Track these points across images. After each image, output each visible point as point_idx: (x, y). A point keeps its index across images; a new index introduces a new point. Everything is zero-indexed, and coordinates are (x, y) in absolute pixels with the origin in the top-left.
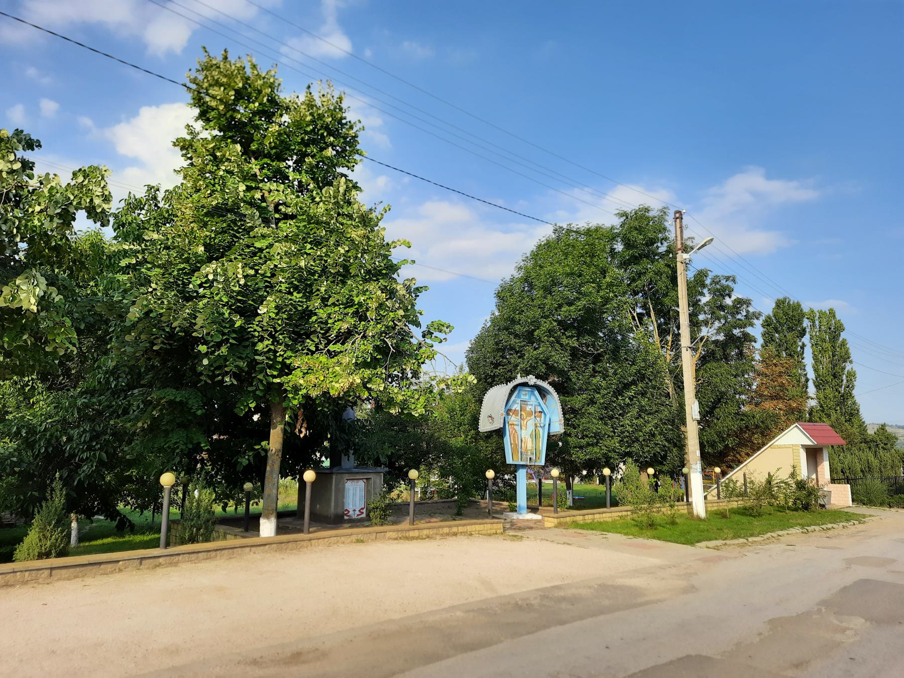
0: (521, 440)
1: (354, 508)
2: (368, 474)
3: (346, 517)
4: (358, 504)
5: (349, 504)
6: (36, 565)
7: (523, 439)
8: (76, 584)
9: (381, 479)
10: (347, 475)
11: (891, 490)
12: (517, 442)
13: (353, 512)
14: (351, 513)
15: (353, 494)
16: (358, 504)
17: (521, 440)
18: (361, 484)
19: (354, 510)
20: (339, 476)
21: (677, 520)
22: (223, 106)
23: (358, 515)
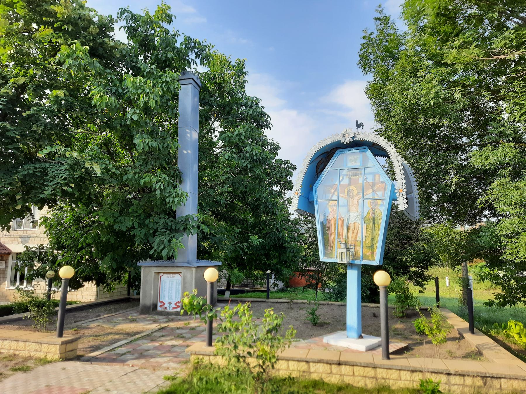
0: (348, 227)
1: (170, 301)
2: (178, 269)
3: (159, 309)
4: (174, 297)
5: (164, 296)
6: (139, 326)
7: (352, 226)
8: (349, 360)
9: (192, 274)
10: (155, 268)
11: (251, 315)
12: (340, 231)
13: (168, 305)
14: (167, 305)
15: (169, 288)
16: (174, 297)
17: (348, 227)
18: (178, 278)
19: (170, 303)
20: (147, 269)
21: (219, 385)
22: (13, 63)
23: (174, 308)
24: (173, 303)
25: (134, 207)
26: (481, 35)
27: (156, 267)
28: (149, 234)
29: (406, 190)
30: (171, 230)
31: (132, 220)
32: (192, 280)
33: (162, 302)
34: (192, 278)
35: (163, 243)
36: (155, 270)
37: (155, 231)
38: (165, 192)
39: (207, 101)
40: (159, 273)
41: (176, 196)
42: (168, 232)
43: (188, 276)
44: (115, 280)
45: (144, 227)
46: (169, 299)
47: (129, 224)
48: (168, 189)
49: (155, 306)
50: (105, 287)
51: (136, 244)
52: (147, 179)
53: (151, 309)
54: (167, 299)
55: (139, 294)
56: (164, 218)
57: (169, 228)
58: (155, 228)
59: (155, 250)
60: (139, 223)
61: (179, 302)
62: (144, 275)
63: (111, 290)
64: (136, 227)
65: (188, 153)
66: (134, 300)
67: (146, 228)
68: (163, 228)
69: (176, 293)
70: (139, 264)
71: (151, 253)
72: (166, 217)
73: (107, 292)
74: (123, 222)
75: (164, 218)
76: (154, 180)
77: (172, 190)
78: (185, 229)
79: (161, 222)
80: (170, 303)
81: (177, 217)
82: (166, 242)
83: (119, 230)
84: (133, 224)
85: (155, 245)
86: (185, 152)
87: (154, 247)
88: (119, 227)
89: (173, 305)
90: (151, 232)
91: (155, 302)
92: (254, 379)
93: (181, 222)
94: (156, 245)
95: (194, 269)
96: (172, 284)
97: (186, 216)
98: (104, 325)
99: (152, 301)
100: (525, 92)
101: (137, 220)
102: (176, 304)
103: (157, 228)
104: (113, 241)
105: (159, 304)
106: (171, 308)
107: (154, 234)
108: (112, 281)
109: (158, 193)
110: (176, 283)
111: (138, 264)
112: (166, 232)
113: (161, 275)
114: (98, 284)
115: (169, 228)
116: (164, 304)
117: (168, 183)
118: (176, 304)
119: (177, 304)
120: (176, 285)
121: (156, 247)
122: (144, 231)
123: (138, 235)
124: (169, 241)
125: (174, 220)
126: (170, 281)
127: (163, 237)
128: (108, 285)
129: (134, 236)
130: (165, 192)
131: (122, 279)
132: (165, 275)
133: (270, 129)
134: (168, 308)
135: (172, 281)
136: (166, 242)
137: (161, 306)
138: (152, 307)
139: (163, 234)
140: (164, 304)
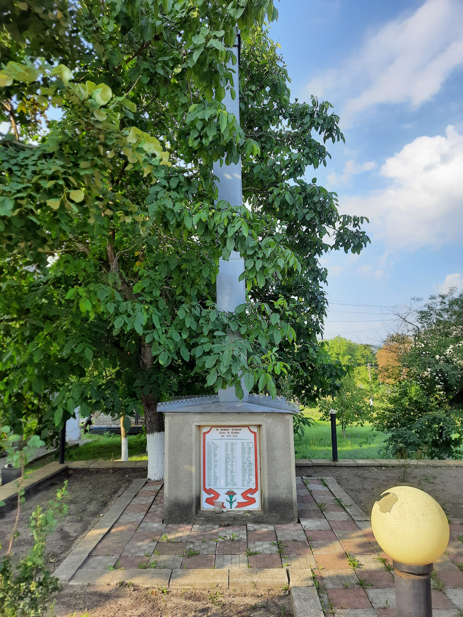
1: (230, 488)
2: (253, 417)
3: (205, 506)
4: (238, 479)
9: (287, 428)
10: (198, 417)
14: (223, 498)
15: (227, 458)
16: (238, 479)
19: (231, 494)
20: (179, 419)
23: (240, 505)
26: (143, 239)
33: (209, 491)
36: (197, 420)
54: (223, 482)
61: (252, 491)
69: (244, 470)
70: (160, 408)
74: (131, 313)
80: (231, 494)
84: (150, 319)
89: (239, 498)
92: (9, 577)
96: (232, 450)
100: (1, 321)
102: (244, 495)
105: (204, 496)
106: (235, 504)
110: (243, 449)
113: (205, 430)
118: (244, 495)
119: (249, 495)
132: (214, 429)
134: (227, 505)
135: (233, 444)
140: (217, 495)
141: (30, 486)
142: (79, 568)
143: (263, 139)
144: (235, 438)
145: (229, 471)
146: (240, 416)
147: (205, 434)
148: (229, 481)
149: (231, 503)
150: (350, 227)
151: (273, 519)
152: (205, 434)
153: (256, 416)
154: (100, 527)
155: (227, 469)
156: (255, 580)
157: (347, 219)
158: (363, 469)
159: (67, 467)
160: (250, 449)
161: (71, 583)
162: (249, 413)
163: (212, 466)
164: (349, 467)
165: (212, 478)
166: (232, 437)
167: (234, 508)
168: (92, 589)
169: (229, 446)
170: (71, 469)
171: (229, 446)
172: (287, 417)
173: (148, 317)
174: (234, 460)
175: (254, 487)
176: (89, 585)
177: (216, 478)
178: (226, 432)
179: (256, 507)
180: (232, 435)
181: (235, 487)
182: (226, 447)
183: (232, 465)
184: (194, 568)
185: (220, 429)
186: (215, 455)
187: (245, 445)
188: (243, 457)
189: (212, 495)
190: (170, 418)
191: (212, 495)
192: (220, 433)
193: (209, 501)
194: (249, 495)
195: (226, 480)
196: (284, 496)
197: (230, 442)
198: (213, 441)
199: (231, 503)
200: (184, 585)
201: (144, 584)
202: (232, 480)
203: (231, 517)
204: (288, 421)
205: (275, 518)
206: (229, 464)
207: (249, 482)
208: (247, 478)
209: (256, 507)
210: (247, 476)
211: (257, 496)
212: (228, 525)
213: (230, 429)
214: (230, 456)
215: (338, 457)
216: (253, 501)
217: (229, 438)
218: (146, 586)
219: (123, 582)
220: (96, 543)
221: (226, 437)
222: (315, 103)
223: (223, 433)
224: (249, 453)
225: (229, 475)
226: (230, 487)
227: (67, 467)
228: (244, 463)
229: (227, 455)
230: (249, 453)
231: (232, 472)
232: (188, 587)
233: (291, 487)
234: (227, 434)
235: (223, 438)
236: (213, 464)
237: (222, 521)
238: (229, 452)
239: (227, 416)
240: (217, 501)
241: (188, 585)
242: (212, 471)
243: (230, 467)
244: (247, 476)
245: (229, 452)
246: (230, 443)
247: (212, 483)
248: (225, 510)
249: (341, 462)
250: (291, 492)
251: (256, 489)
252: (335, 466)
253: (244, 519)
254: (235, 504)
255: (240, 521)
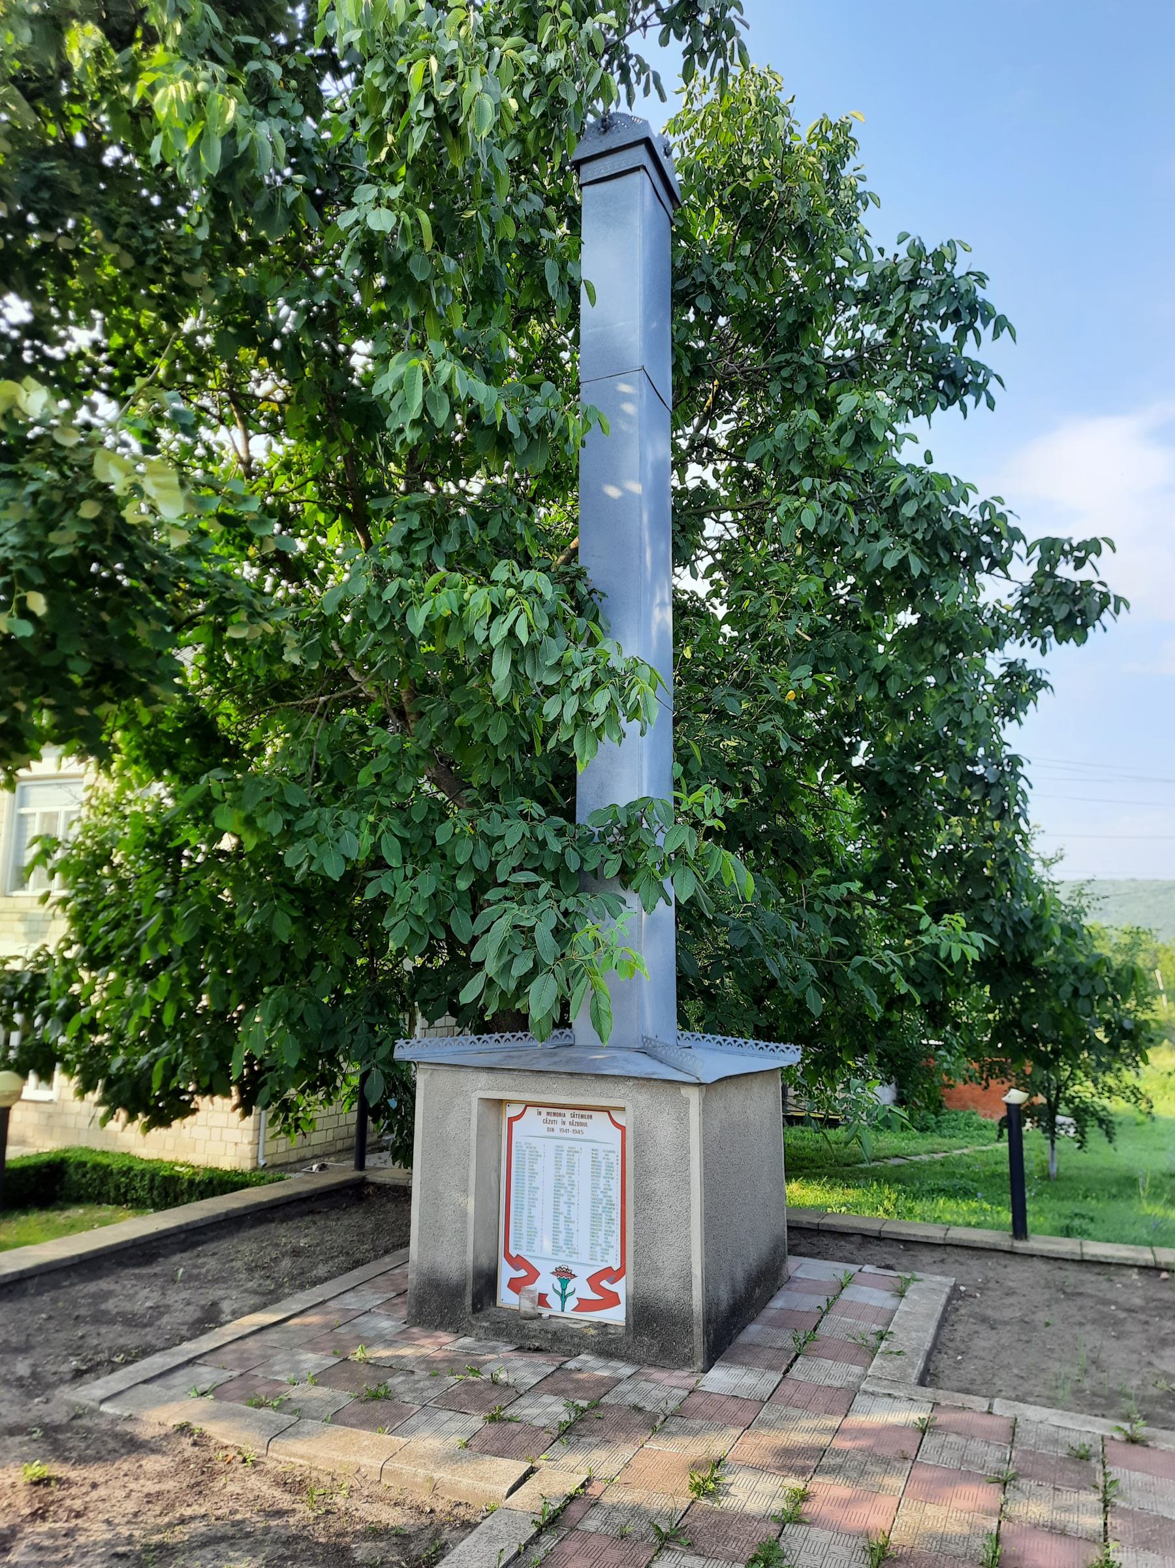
2: (600, 1086)
3: (507, 1298)
4: (582, 1240)
9: (682, 1119)
10: (484, 1078)
14: (546, 1283)
15: (558, 1185)
16: (582, 1240)
19: (564, 1275)
20: (445, 1078)
24: (583, 1273)
25: (381, 764)
27: (490, 1069)
28: (452, 898)
29: (387, 923)
30: (559, 875)
31: (374, 828)
32: (685, 1159)
33: (517, 1262)
34: (684, 1146)
35: (531, 943)
36: (483, 1087)
37: (484, 882)
38: (536, 665)
39: (701, 278)
40: (500, 1102)
41: (596, 684)
42: (545, 888)
43: (663, 1127)
44: (313, 1088)
45: (426, 860)
46: (557, 1249)
47: (359, 846)
48: (554, 650)
49: (487, 1283)
50: (275, 1117)
51: (392, 946)
52: (445, 604)
53: (468, 1301)
54: (547, 1245)
55: (404, 1154)
56: (524, 816)
57: (549, 866)
58: (482, 864)
59: (490, 982)
60: (404, 842)
62: (426, 1108)
63: (297, 1127)
64: (393, 863)
65: (627, 494)
66: (382, 1189)
67: (436, 865)
68: (520, 868)
69: (595, 1216)
71: (467, 996)
72: (537, 810)
73: (282, 1135)
75: (524, 816)
76: (479, 599)
77: (574, 655)
78: (626, 875)
79: (514, 832)
80: (564, 1275)
81: (582, 816)
82: (543, 935)
83: (310, 874)
84: (376, 847)
85: (487, 952)
86: (613, 492)
87: (480, 966)
88: (312, 858)
89: (581, 1289)
90: (463, 885)
91: (484, 1261)
93: (603, 836)
94: (492, 951)
95: (693, 1096)
96: (571, 1165)
97: (631, 806)
98: (216, 1431)
99: (470, 1264)
101: (395, 823)
102: (594, 1281)
103: (493, 865)
104: (284, 930)
105: (506, 1273)
106: (572, 1302)
107: (475, 901)
108: (303, 1092)
109: (501, 668)
110: (595, 1162)
111: (398, 1054)
112: (537, 885)
113: (513, 1111)
114: (246, 1107)
115: (549, 866)
116: (533, 1274)
117: (552, 618)
118: (594, 1281)
119: (605, 1284)
120: (595, 1174)
121: (491, 968)
122: (428, 883)
123: (399, 900)
124: (561, 934)
125: (570, 828)
126: (559, 1149)
127: (524, 915)
128: (287, 1107)
129: (381, 905)
130: (536, 665)
131: (338, 1083)
133: (991, 404)
134: (554, 1300)
135: (572, 1152)
136: (543, 935)
137: (515, 1285)
138: (469, 1289)
139: (523, 894)
140: (533, 1274)
141: (246, 1208)
142: (145, 1382)
143: (785, 373)
144: (578, 1136)
145: (562, 1218)
146: (576, 1082)
147: (511, 1120)
148: (561, 1243)
149: (564, 1297)
150: (1065, 571)
151: (641, 1353)
152: (511, 1120)
153: (611, 1086)
154: (275, 1312)
155: (556, 1213)
156: (436, 1476)
157: (1051, 549)
158: (1097, 1269)
159: (364, 1178)
160: (610, 1167)
161: (104, 1408)
162: (596, 1076)
163: (526, 1203)
164: (1056, 1259)
165: (524, 1230)
166: (570, 1135)
167: (569, 1312)
168: (129, 1428)
169: (564, 1154)
170: (373, 1184)
171: (564, 1154)
172: (686, 1092)
173: (372, 840)
174: (575, 1192)
175: (616, 1266)
176: (130, 1418)
177: (533, 1233)
178: (559, 1119)
179: (616, 1316)
180: (571, 1128)
181: (574, 1258)
182: (558, 1156)
183: (569, 1204)
184: (352, 1426)
185: (544, 1111)
186: (533, 1175)
187: (601, 1155)
188: (595, 1187)
189: (522, 1273)
190: (427, 1076)
191: (522, 1273)
192: (545, 1121)
193: (515, 1285)
194: (605, 1284)
195: (555, 1240)
196: (671, 1296)
197: (566, 1144)
198: (530, 1140)
199: (564, 1297)
200: (295, 1455)
201: (223, 1435)
202: (568, 1242)
203: (547, 1332)
204: (687, 1102)
205: (649, 1350)
206: (563, 1199)
207: (605, 1252)
208: (601, 1240)
209: (616, 1316)
210: (601, 1234)
211: (620, 1288)
212: (538, 1350)
213: (568, 1112)
214: (565, 1181)
215: (1029, 1227)
216: (611, 1300)
217: (565, 1135)
218: (226, 1442)
219: (188, 1425)
220: (229, 1339)
221: (557, 1133)
222: (917, 252)
223: (552, 1122)
224: (609, 1177)
225: (562, 1227)
226: (562, 1256)
227: (364, 1178)
228: (595, 1203)
229: (559, 1178)
230: (609, 1177)
231: (568, 1220)
232: (302, 1462)
233: (689, 1275)
234: (559, 1125)
235: (551, 1134)
236: (526, 1196)
237: (527, 1337)
238: (563, 1171)
239: (545, 1081)
240: (531, 1287)
241: (302, 1457)
242: (525, 1213)
243: (563, 1208)
244: (601, 1234)
245: (563, 1171)
246: (566, 1149)
247: (524, 1242)
248: (546, 1313)
249: (1037, 1243)
250: (688, 1287)
251: (621, 1272)
252: (1012, 1253)
253: (576, 1340)
254: (572, 1302)
255: (567, 1344)
